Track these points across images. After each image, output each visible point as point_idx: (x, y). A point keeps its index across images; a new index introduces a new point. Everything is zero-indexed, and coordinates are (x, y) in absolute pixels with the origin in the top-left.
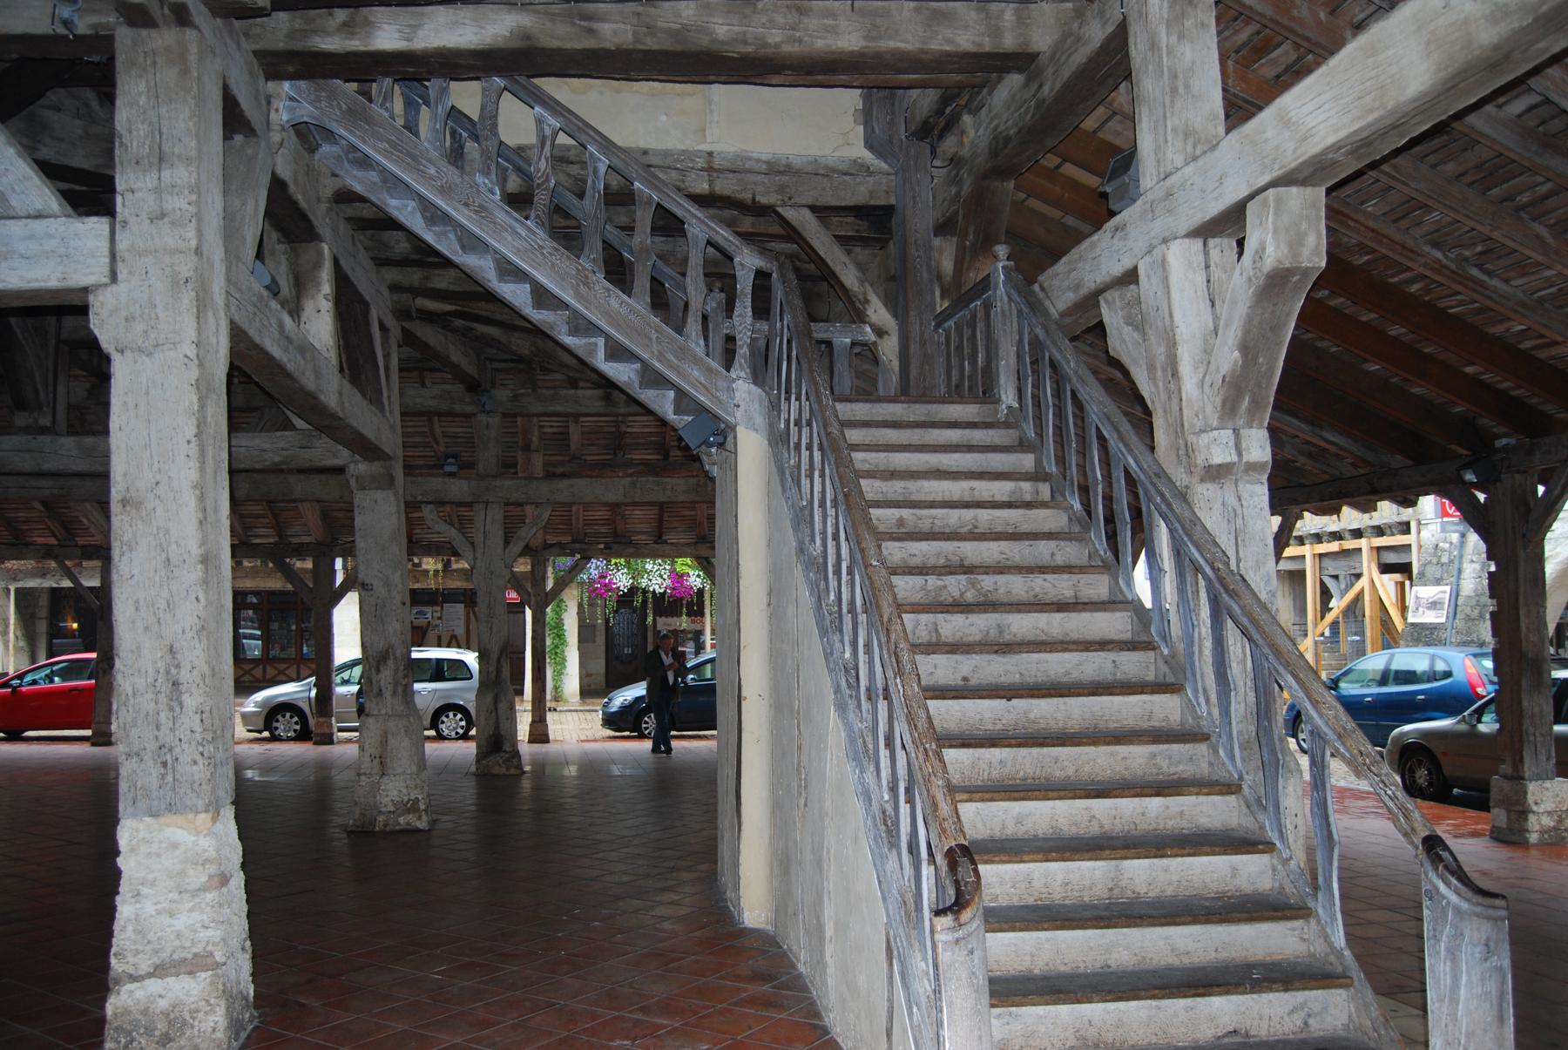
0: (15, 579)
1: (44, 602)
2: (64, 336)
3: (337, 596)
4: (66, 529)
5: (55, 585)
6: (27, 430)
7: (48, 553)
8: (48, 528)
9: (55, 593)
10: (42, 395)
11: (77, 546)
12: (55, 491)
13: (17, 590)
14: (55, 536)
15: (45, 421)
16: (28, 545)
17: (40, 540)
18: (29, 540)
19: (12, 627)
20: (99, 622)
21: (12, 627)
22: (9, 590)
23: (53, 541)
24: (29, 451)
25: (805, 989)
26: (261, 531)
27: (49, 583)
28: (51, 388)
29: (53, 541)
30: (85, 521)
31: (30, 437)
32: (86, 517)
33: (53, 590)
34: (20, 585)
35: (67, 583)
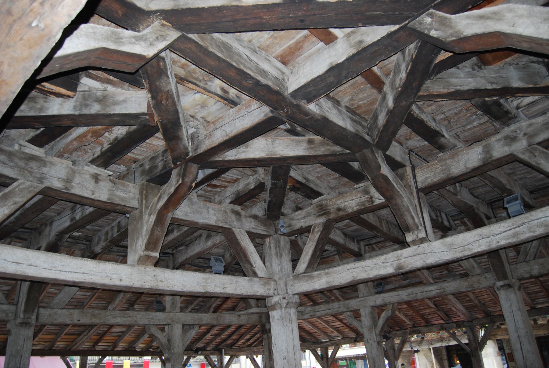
0: (432, 344)
1: (444, 353)
2: (420, 186)
3: (481, 345)
4: (447, 315)
5: (447, 345)
6: (414, 242)
7: (442, 328)
8: (439, 316)
9: (448, 348)
10: (416, 220)
11: (453, 322)
12: (438, 291)
13: (433, 348)
14: (443, 319)
15: (422, 235)
16: (432, 325)
17: (437, 322)
18: (433, 323)
19: (435, 364)
20: (472, 358)
21: (435, 364)
22: (430, 349)
23: (442, 322)
24: (418, 255)
25: (70, 255)
26: (541, 300)
27: (444, 344)
28: (420, 216)
29: (442, 322)
30: (454, 309)
31: (416, 247)
32: (454, 307)
33: (447, 347)
34: (434, 346)
35: (454, 343)
